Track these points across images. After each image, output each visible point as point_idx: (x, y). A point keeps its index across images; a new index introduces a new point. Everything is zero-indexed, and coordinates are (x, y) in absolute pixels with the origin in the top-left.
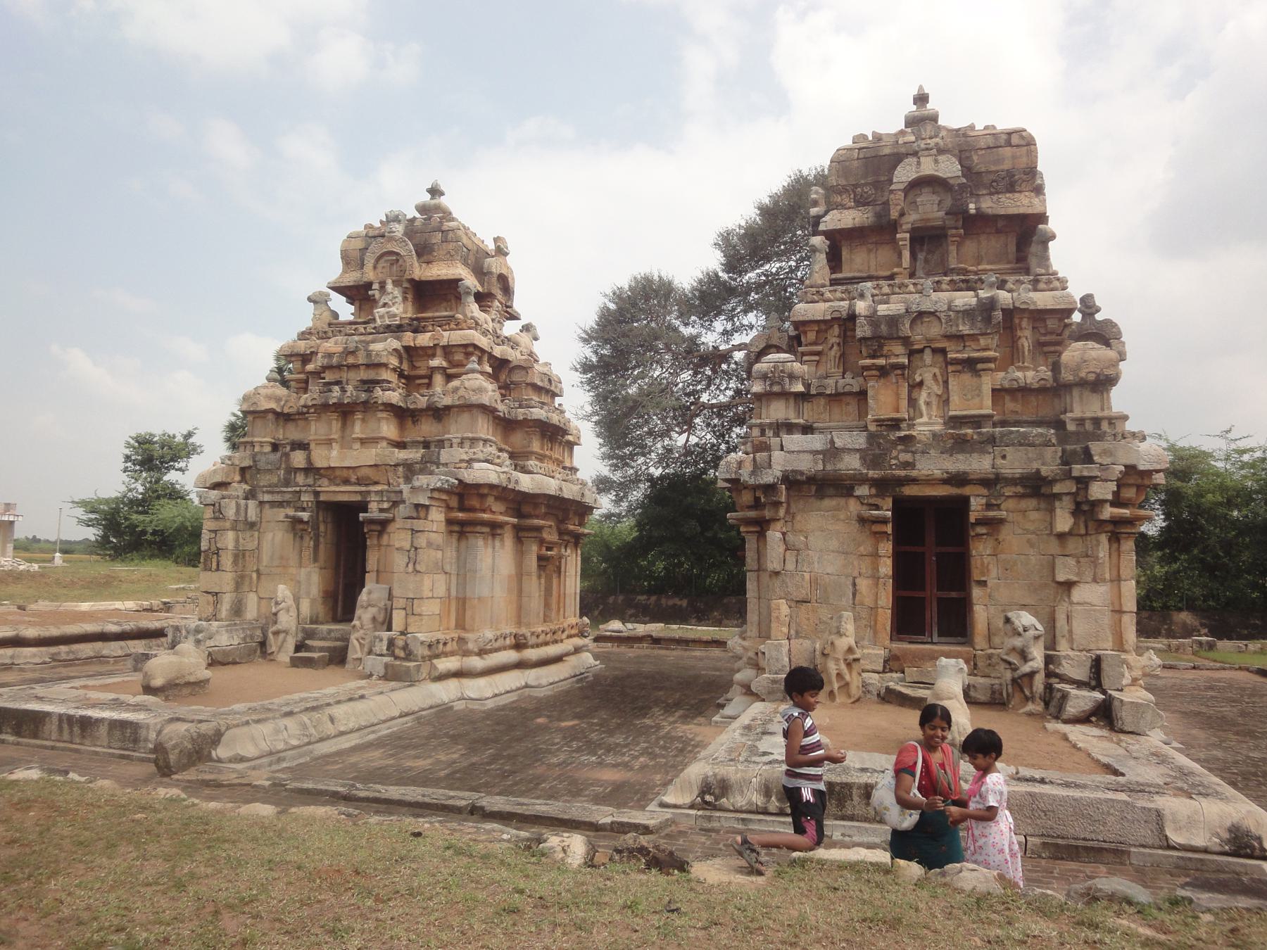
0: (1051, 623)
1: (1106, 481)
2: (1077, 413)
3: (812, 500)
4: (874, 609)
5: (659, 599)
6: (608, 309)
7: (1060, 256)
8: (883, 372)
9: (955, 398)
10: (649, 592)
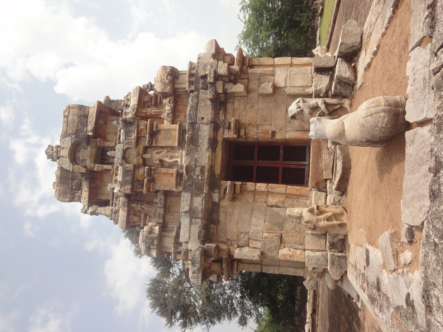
0: (294, 97)
1: (217, 66)
2: (187, 85)
3: (219, 227)
4: (287, 196)
5: (297, 300)
6: (158, 311)
7: (117, 95)
8: (152, 180)
9: (170, 143)
10: (294, 303)
